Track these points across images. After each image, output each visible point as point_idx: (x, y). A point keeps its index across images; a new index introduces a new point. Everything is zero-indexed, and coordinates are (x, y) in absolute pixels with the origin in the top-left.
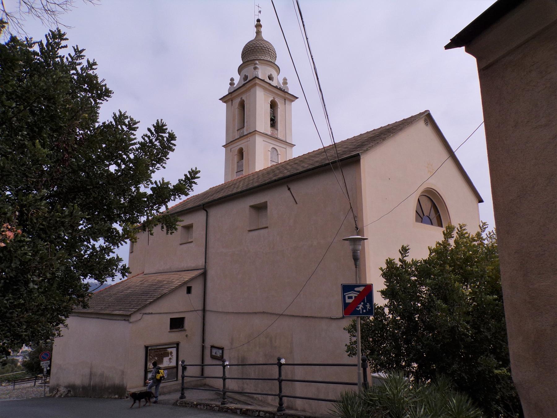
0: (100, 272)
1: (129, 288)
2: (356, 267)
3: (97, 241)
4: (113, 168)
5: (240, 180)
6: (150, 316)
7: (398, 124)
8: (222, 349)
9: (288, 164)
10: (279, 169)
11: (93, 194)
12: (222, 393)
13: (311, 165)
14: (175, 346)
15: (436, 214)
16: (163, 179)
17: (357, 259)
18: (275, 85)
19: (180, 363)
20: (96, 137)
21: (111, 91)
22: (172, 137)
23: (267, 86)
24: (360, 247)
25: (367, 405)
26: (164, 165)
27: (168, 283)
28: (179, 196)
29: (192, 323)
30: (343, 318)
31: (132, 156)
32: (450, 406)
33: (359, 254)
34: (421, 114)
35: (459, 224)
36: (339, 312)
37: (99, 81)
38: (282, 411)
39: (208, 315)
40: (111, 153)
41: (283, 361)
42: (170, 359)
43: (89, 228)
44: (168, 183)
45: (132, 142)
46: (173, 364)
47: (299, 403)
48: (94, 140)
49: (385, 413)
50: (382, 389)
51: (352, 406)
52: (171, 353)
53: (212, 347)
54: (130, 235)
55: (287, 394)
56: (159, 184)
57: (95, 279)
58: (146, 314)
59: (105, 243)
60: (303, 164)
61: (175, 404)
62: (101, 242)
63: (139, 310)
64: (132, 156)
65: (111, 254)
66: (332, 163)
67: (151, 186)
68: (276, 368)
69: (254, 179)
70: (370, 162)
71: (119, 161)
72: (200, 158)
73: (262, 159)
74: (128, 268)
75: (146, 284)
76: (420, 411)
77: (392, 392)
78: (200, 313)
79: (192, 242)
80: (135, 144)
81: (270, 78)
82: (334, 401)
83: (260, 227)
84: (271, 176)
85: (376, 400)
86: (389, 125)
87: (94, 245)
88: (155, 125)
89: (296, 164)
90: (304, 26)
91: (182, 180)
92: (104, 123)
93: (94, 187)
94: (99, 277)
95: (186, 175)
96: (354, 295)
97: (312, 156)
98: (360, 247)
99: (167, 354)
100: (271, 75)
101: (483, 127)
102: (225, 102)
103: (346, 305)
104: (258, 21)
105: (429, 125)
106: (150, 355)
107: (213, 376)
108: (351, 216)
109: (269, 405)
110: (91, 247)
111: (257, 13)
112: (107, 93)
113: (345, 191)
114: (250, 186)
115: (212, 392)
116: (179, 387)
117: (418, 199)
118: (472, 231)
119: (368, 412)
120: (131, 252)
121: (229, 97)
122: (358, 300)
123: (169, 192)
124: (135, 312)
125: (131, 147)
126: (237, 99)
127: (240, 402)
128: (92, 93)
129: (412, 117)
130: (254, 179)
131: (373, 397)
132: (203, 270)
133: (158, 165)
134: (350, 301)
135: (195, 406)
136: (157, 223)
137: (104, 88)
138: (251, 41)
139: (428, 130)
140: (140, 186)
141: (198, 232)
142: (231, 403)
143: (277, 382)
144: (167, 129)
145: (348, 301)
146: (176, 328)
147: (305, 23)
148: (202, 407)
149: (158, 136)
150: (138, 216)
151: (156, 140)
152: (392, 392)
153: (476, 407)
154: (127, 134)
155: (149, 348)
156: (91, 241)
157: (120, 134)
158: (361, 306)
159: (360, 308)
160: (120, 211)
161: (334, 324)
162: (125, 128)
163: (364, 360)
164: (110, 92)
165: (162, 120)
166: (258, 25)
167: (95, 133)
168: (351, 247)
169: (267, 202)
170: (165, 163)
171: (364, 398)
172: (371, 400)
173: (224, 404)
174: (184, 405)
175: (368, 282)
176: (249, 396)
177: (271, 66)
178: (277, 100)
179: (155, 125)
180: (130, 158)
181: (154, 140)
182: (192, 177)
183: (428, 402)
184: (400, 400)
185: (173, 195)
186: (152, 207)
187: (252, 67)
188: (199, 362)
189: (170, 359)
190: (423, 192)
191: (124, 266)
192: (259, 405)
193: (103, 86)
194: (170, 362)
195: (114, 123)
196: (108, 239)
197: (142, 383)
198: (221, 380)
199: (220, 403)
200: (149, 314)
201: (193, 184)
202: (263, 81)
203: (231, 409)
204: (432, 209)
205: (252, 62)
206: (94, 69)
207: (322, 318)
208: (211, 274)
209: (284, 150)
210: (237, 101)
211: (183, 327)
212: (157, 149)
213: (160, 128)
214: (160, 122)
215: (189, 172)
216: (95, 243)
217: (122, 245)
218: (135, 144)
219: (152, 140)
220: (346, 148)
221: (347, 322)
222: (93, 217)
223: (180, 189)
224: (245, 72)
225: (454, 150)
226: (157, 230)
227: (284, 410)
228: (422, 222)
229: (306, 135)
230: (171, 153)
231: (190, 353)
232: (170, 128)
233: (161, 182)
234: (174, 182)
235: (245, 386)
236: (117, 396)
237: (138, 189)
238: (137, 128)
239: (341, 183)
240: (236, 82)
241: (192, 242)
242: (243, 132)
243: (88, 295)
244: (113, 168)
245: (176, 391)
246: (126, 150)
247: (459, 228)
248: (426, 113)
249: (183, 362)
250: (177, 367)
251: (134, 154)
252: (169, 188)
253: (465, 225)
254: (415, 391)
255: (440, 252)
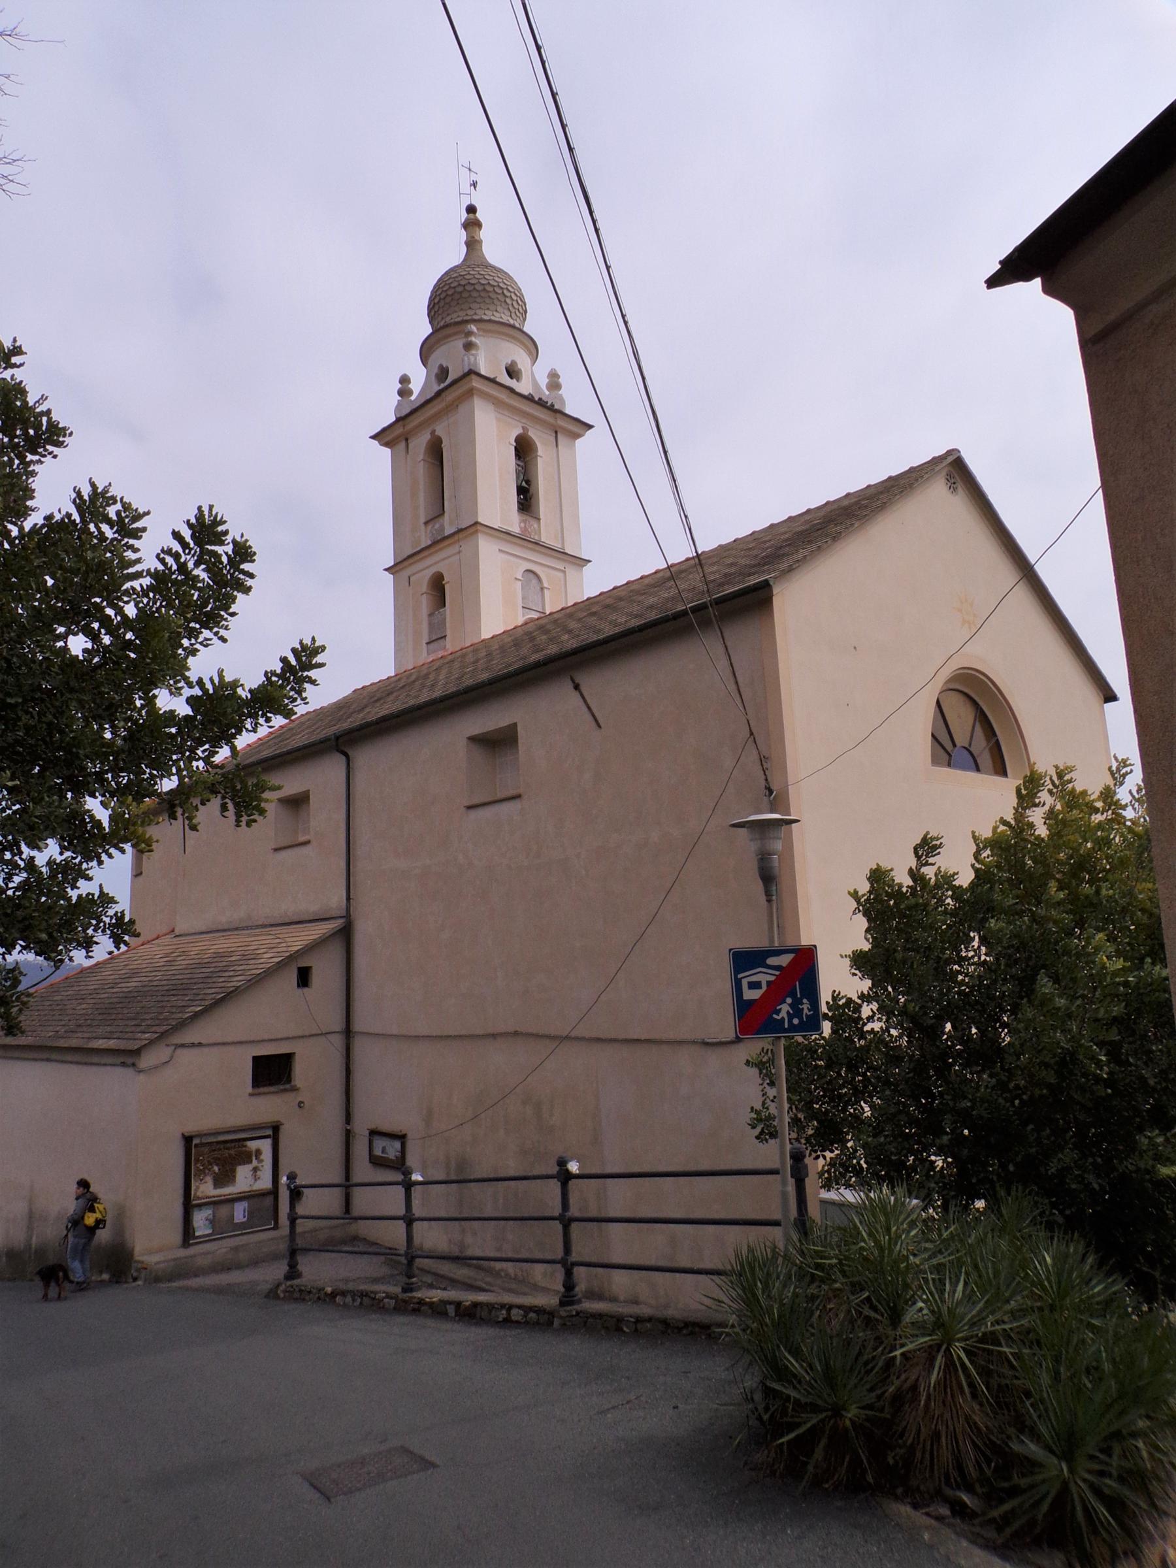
0: (50, 935)
1: (133, 974)
2: (769, 901)
3: (40, 849)
4: (78, 645)
5: (438, 664)
6: (195, 1051)
7: (872, 490)
8: (402, 1138)
9: (571, 616)
10: (547, 632)
11: (25, 718)
12: (403, 1260)
13: (637, 616)
14: (270, 1132)
15: (988, 740)
16: (220, 673)
17: (771, 878)
18: (526, 393)
19: (284, 1180)
20: (27, 559)
21: (64, 429)
22: (243, 552)
23: (503, 396)
24: (778, 846)
25: (808, 1279)
26: (222, 632)
27: (246, 958)
28: (268, 720)
29: (315, 1067)
30: (738, 1040)
31: (131, 611)
32: (1037, 1274)
33: (776, 864)
34: (936, 461)
35: (1057, 767)
36: (725, 1024)
37: (31, 400)
38: (571, 1303)
39: (358, 1044)
40: (70, 602)
41: (573, 1167)
42: (255, 1169)
43: (15, 812)
44: (235, 684)
45: (131, 570)
46: (265, 1183)
47: (620, 1281)
48: (22, 567)
49: (856, 1299)
50: (849, 1235)
51: (766, 1287)
52: (258, 1152)
53: (374, 1133)
54: (133, 833)
55: (587, 1259)
56: (209, 686)
57: (37, 954)
58: (183, 1046)
59: (61, 854)
60: (613, 617)
61: (272, 1294)
62: (50, 852)
63: (163, 1035)
64: (131, 611)
65: (81, 883)
66: (695, 610)
67: (187, 692)
68: (555, 1186)
69: (477, 661)
70: (797, 603)
71: (96, 625)
72: (324, 610)
73: (500, 603)
74: (132, 922)
75: (181, 963)
76: (954, 1292)
77: (876, 1241)
78: (338, 1041)
79: (307, 843)
80: (138, 575)
81: (512, 372)
82: (718, 1273)
83: (499, 796)
84: (525, 651)
85: (831, 1266)
86: (848, 495)
87: (32, 858)
88: (193, 521)
89: (594, 614)
90: (597, 231)
91: (274, 673)
92: (49, 518)
93: (25, 701)
94: (46, 949)
95: (284, 660)
96: (764, 977)
97: (639, 593)
98: (778, 846)
99: (246, 1157)
100: (514, 363)
101: (1098, 505)
102: (386, 445)
103: (744, 1008)
104: (471, 209)
105: (960, 490)
106: (197, 1160)
107: (377, 1214)
108: (751, 757)
109: (536, 1288)
110: (22, 864)
111: (466, 187)
112: (54, 435)
113: (732, 687)
114: (468, 682)
115: (375, 1259)
116: (283, 1247)
117: (938, 702)
118: (1089, 782)
119: (813, 1298)
120: (137, 874)
121: (399, 430)
122: (777, 991)
123: (240, 707)
124: (152, 1042)
125: (127, 585)
126: (421, 433)
127: (454, 1283)
128: (12, 437)
129: (912, 470)
130: (477, 661)
131: (825, 1258)
132: (342, 921)
133: (206, 633)
134: (755, 995)
135: (329, 1298)
136: (207, 795)
137: (44, 419)
138: (452, 270)
139: (958, 505)
140: (156, 692)
141: (325, 816)
142: (431, 1286)
143: (557, 1226)
144: (226, 533)
145: (750, 995)
146: (271, 1084)
147: (600, 224)
148: (349, 1299)
149: (203, 552)
150: (152, 776)
151: (197, 565)
152: (876, 1241)
153: (1109, 1274)
154: (115, 547)
155: (196, 1141)
156: (24, 848)
157: (94, 548)
158: (785, 1008)
159: (783, 1014)
160: (102, 763)
161: (714, 1059)
162: (109, 533)
163: (797, 1157)
164: (63, 431)
165: (211, 507)
166: (472, 223)
167: (25, 548)
168: (753, 847)
169: (515, 724)
170: (226, 628)
171: (799, 1259)
172: (818, 1266)
173: (411, 1290)
174: (297, 1295)
175: (805, 941)
176: (479, 1268)
177: (513, 337)
178: (535, 434)
179: (193, 521)
180: (125, 617)
181: (190, 565)
182: (302, 663)
183: (976, 1267)
184: (896, 1263)
185: (250, 715)
186: (193, 750)
187: (459, 343)
188: (336, 1176)
189: (255, 1169)
190: (949, 681)
191: (119, 917)
192: (510, 1291)
193: (42, 414)
194: (256, 1179)
195: (76, 517)
196: (70, 843)
197: (177, 1237)
198: (401, 1225)
199: (397, 1290)
200: (193, 1045)
201: (306, 685)
202: (493, 381)
203: (431, 1304)
204: (977, 724)
205: (461, 327)
206: (15, 366)
207: (681, 1042)
208: (364, 930)
209: (560, 575)
210: (421, 442)
211: (289, 1081)
212: (199, 589)
213: (206, 530)
214: (206, 513)
215: (294, 650)
216: (34, 853)
217: (110, 856)
218: (138, 575)
219: (185, 563)
220: (732, 564)
221: (753, 1047)
222: (27, 782)
223: (268, 699)
224: (440, 357)
225: (1032, 561)
226: (209, 813)
227: (579, 1301)
228: (949, 765)
229: (620, 532)
230: (240, 596)
231: (311, 1152)
232: (234, 529)
233: (216, 681)
234: (251, 680)
235: (469, 1240)
236: (105, 1276)
237: (150, 701)
238: (144, 530)
239: (723, 663)
240: (416, 386)
241: (307, 843)
242: (442, 528)
243: (18, 998)
244: (78, 645)
245: (275, 1257)
246: (113, 594)
247: (1055, 778)
248: (950, 459)
249: (292, 1177)
250: (274, 1192)
251: (136, 605)
252: (240, 697)
253: (1071, 769)
254: (940, 1235)
255: (1007, 849)
